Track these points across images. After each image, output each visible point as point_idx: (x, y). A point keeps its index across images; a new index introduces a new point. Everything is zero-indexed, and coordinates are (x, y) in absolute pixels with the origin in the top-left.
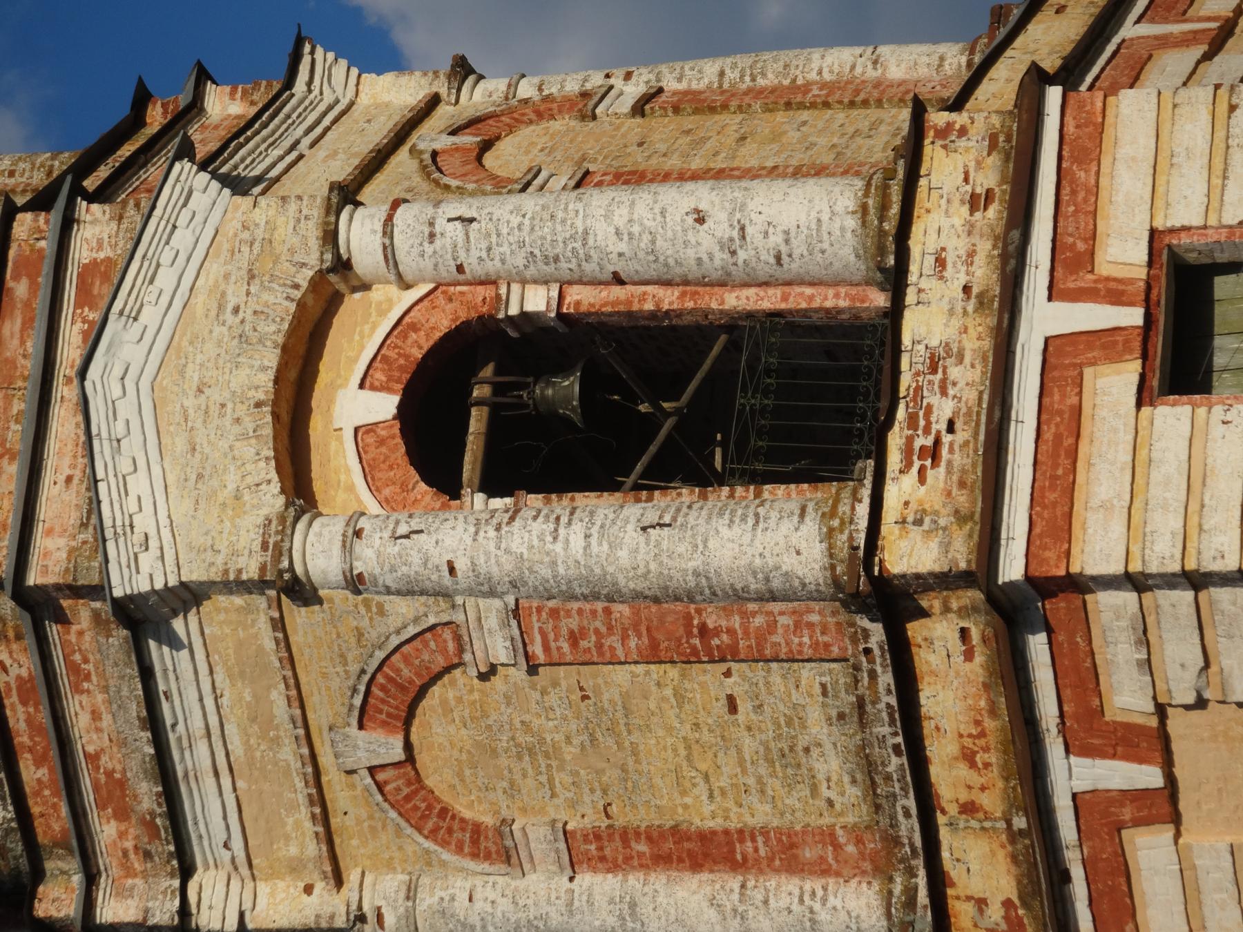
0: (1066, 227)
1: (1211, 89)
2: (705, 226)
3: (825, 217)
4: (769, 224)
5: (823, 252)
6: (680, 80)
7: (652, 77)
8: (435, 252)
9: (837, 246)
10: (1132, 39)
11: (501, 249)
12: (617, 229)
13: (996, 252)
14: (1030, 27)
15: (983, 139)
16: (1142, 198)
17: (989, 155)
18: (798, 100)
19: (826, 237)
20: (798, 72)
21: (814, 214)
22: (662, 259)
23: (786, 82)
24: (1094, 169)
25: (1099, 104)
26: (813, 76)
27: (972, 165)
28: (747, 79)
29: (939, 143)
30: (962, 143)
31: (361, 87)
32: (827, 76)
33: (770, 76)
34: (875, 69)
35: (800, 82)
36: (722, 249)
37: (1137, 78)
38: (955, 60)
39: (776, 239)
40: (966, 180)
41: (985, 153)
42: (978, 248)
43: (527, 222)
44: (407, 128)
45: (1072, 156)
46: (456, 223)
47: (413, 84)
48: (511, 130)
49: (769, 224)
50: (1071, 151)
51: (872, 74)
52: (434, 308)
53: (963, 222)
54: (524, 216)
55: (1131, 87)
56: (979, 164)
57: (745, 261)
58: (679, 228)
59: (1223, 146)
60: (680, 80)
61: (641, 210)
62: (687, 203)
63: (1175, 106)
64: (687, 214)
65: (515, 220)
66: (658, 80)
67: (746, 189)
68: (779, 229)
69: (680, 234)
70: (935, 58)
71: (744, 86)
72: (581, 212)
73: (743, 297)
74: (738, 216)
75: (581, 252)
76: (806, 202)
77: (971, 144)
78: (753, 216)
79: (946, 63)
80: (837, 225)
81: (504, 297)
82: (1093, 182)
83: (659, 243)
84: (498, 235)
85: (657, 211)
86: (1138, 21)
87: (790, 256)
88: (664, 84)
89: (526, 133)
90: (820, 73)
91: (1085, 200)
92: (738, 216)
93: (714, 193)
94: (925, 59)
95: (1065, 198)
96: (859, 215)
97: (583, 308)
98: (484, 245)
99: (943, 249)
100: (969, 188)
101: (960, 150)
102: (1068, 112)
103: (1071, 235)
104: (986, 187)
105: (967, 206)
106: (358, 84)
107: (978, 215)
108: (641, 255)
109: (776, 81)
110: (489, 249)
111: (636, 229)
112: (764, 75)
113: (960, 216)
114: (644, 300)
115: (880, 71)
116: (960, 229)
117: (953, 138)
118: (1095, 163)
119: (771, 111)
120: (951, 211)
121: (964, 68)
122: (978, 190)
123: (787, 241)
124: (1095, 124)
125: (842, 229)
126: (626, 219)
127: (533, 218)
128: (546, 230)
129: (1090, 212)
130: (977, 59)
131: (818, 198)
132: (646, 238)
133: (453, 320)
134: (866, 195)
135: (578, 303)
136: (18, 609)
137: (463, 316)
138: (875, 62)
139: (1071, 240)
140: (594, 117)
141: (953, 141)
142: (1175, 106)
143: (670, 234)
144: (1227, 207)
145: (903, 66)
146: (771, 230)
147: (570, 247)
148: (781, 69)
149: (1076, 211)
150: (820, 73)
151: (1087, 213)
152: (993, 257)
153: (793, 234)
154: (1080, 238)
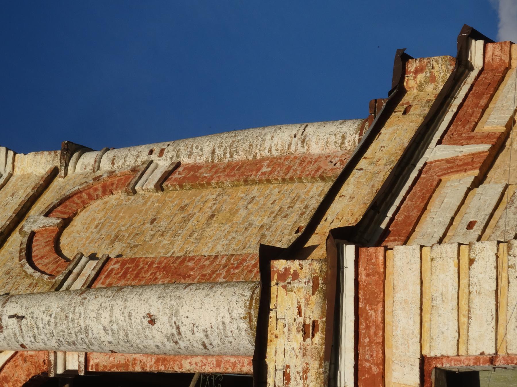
0: (364, 355)
1: (455, 246)
2: (156, 326)
3: (227, 321)
4: (194, 325)
5: (231, 343)
6: (190, 156)
7: (174, 153)
8: (5, 338)
9: (238, 339)
10: (431, 163)
11: (42, 337)
12: (104, 327)
13: (321, 370)
14: (383, 131)
15: (309, 281)
16: (413, 332)
17: (313, 294)
18: (252, 177)
19: (230, 334)
20: (257, 150)
21: (220, 319)
22: (135, 345)
23: (251, 158)
24: (381, 309)
25: (381, 258)
26: (266, 153)
27: (303, 301)
28: (228, 155)
29: (281, 284)
30: (295, 284)
31: (16, 163)
32: (275, 153)
33: (241, 153)
34: (303, 147)
35: (259, 157)
36: (168, 340)
37: (408, 238)
38: (352, 138)
39: (199, 335)
40: (300, 313)
41: (311, 292)
42: (310, 367)
43: (53, 320)
44: (29, 204)
45: (365, 299)
46: (14, 319)
47: (43, 160)
48: (84, 205)
49: (194, 325)
50: (365, 295)
51: (301, 150)
52: (17, 366)
53: (299, 346)
54: (51, 316)
55: (405, 244)
56: (307, 300)
57: (185, 347)
58: (140, 327)
59: (467, 291)
60: (190, 156)
61: (117, 314)
62: (143, 310)
63: (432, 259)
64: (144, 317)
65: (46, 319)
66: (178, 157)
67: (179, 298)
68: (200, 328)
69: (141, 331)
70: (340, 136)
71: (226, 161)
72: (82, 314)
73: (194, 363)
74: (174, 319)
75: (86, 340)
76: (214, 309)
77: (302, 285)
78: (184, 320)
79: (346, 141)
80: (235, 327)
81: (53, 363)
82: (380, 319)
83: (130, 336)
84: (38, 328)
85: (126, 314)
86: (439, 142)
87: (211, 344)
88: (180, 159)
89: (94, 206)
90: (270, 151)
91: (376, 334)
92: (174, 319)
93: (160, 301)
94: (333, 138)
95: (362, 331)
96: (248, 320)
97: (101, 369)
98: (31, 334)
99: (288, 366)
100: (301, 319)
101: (294, 290)
102: (361, 263)
103: (368, 361)
104: (312, 319)
105: (301, 333)
106: (14, 161)
107: (308, 340)
108: (122, 343)
109: (245, 157)
110: (35, 337)
111: (115, 327)
112: (237, 152)
113: (297, 341)
114: (135, 364)
115: (306, 149)
116: (298, 351)
117: (290, 280)
118: (380, 304)
119: (237, 186)
120: (291, 337)
121: (357, 141)
122: (308, 322)
123: (207, 336)
124: (379, 273)
125: (239, 329)
126: (108, 320)
127: (56, 318)
128: (64, 326)
129: (379, 343)
130: (364, 136)
131: (222, 306)
132: (122, 333)
133: (28, 375)
134: (250, 308)
135: (97, 365)
136: (60, 281)
137: (33, 372)
138: (303, 142)
139: (368, 365)
140: (135, 192)
141: (289, 283)
142: (432, 259)
143: (135, 331)
144: (471, 341)
145: (320, 144)
146: (195, 329)
147: (79, 338)
148: (247, 148)
149: (370, 342)
150: (270, 151)
151: (377, 344)
152: (320, 373)
153: (209, 332)
154: (373, 363)
